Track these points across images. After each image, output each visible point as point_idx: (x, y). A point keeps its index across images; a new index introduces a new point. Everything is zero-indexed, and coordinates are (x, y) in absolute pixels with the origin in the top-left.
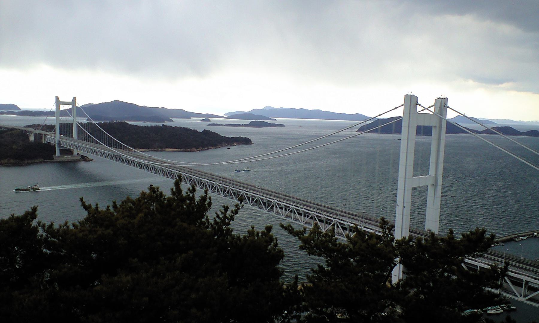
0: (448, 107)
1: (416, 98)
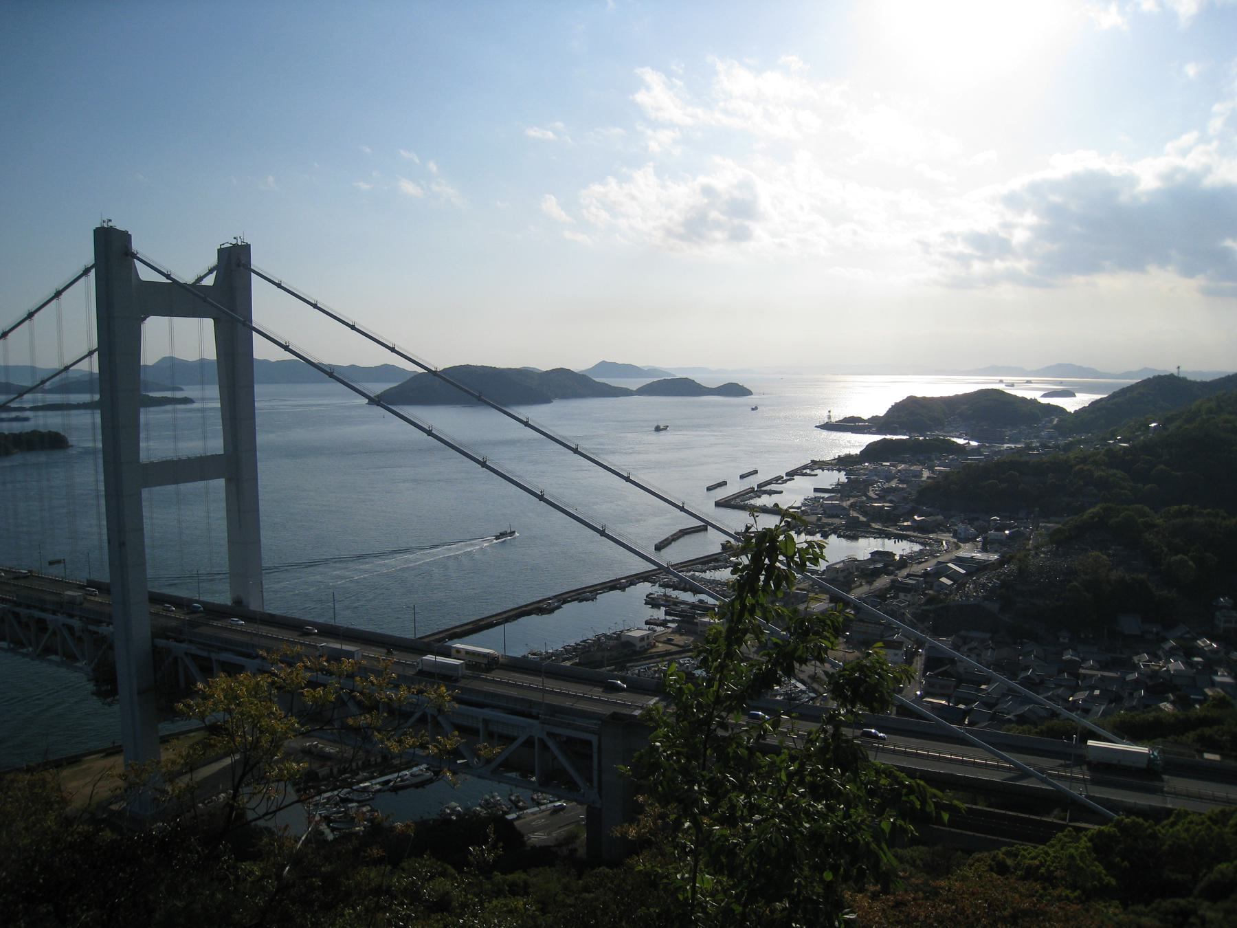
0: (134, 256)
1: (125, 237)
